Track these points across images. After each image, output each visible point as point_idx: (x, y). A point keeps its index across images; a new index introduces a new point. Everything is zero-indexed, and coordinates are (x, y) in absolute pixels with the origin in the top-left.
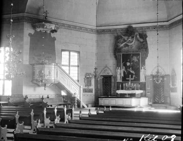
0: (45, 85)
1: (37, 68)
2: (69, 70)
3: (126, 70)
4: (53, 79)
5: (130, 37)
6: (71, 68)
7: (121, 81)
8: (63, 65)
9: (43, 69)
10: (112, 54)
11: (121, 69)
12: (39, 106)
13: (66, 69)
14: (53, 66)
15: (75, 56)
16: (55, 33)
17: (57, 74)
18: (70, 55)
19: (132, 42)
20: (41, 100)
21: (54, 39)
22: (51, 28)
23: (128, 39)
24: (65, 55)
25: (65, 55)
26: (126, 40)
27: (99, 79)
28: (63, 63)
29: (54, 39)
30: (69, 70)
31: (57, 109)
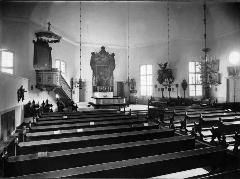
11: (95, 77)
26: (99, 56)
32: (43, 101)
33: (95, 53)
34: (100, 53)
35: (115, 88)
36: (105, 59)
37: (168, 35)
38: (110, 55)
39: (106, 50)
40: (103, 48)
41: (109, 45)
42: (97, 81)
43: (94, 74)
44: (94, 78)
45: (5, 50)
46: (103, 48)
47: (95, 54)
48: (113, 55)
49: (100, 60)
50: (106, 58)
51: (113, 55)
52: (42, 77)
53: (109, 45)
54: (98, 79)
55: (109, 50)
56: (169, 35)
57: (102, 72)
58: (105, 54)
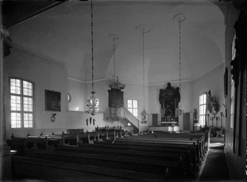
0: (118, 120)
1: (113, 109)
2: (133, 111)
3: (167, 110)
4: (122, 116)
5: (169, 90)
6: (134, 109)
7: (164, 117)
8: (129, 108)
9: (116, 111)
10: (159, 103)
11: (163, 109)
12: (119, 131)
13: (130, 111)
14: (122, 109)
15: (135, 102)
16: (123, 89)
17: (124, 113)
18: (132, 102)
19: (170, 92)
20: (113, 128)
21: (123, 92)
22: (120, 87)
23: (167, 91)
24: (129, 101)
25: (129, 102)
26: (166, 91)
27: (211, 145)
28: (129, 107)
29: (123, 92)
30: (133, 111)
31: (162, 121)
32: (93, 130)
33: (163, 90)
34: (166, 89)
35: (181, 118)
36: (171, 93)
37: (179, 52)
38: (175, 89)
39: (172, 85)
40: (169, 84)
41: (171, 81)
42: (164, 113)
43: (162, 107)
44: (162, 110)
45: (4, 88)
46: (169, 84)
47: (162, 90)
48: (178, 88)
49: (166, 95)
50: (172, 93)
51: (178, 88)
52: (193, 119)
53: (171, 81)
54: (165, 111)
55: (174, 85)
56: (93, 40)
57: (169, 105)
58: (170, 90)
